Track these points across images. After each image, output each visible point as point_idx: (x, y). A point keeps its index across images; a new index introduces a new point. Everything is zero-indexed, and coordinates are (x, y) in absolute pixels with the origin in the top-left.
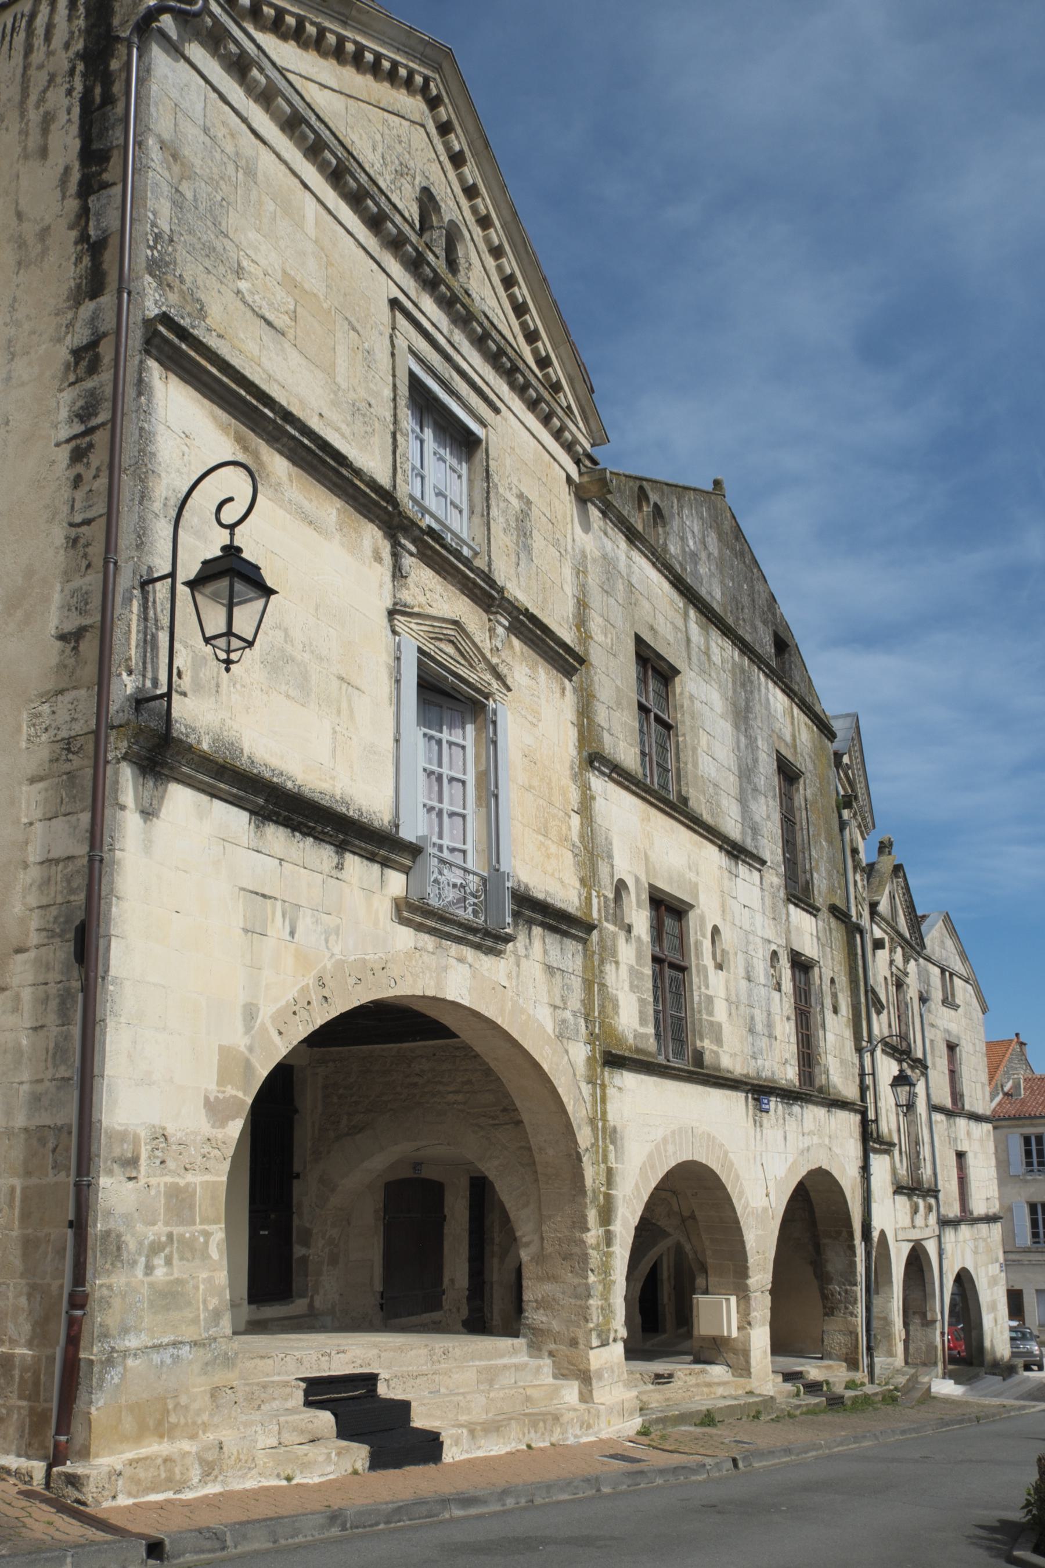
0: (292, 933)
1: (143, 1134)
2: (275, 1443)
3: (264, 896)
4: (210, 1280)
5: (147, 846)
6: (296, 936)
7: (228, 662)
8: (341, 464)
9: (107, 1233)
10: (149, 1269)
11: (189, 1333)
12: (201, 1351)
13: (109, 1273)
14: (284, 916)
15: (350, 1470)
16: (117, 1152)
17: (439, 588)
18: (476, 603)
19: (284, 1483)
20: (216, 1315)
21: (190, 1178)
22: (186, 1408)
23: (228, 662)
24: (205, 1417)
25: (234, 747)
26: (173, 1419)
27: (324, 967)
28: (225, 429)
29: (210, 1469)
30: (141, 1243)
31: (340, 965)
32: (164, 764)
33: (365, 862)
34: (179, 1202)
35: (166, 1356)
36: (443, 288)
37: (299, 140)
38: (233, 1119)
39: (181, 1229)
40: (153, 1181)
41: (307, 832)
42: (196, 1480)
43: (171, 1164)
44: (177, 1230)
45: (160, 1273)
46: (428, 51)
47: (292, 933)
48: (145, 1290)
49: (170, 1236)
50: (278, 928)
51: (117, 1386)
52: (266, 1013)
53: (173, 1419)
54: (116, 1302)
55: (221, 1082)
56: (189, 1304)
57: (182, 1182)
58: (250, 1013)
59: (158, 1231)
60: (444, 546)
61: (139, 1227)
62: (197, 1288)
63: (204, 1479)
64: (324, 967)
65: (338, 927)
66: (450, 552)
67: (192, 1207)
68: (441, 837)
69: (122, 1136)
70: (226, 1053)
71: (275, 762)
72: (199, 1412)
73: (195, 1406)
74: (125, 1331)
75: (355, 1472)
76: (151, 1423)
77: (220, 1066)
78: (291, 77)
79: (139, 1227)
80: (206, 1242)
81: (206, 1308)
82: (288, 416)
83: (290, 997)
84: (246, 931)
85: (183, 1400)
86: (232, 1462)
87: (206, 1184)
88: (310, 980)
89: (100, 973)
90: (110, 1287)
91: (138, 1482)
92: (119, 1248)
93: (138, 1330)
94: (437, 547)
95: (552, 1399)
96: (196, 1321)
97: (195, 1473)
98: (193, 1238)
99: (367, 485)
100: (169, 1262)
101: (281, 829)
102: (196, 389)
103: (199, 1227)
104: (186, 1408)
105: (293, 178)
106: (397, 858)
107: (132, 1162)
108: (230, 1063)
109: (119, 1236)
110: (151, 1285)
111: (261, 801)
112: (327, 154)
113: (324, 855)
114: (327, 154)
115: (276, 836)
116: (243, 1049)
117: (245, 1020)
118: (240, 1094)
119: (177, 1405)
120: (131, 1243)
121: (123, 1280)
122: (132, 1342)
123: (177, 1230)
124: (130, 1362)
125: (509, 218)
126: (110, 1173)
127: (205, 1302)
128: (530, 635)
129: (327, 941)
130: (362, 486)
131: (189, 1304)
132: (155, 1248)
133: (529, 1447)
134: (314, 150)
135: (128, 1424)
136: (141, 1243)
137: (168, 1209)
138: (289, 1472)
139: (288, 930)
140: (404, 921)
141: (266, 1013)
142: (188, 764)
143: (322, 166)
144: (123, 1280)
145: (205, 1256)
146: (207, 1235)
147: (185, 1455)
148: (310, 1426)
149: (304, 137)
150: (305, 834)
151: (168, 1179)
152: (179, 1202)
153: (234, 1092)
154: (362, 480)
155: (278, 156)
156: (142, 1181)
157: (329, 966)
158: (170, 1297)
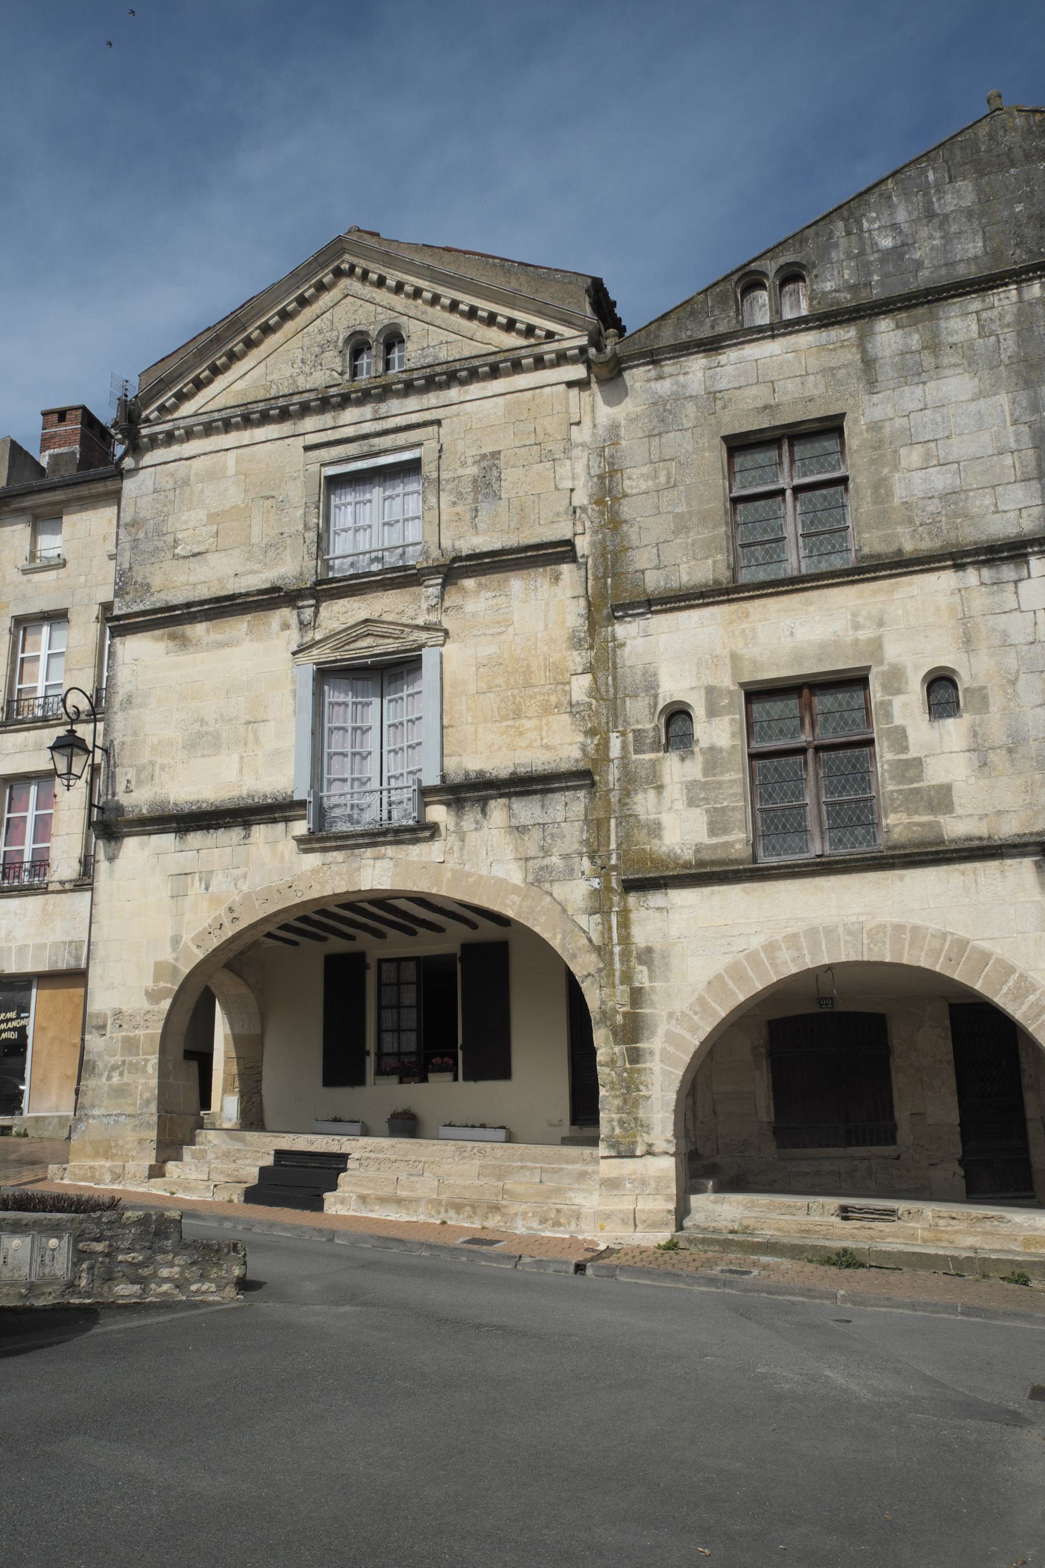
0: (207, 889)
1: (109, 1013)
2: (206, 1178)
3: (186, 874)
4: (146, 1084)
5: (111, 874)
6: (210, 889)
7: (68, 786)
8: (235, 599)
9: (89, 1061)
10: (109, 1078)
11: (129, 1110)
12: (133, 1120)
13: (87, 1079)
14: (200, 880)
15: (227, 1199)
16: (94, 1023)
17: (356, 605)
18: (405, 587)
19: (168, 1195)
20: (148, 1102)
21: (137, 1032)
22: (122, 1147)
23: (68, 786)
24: (134, 1153)
25: (164, 803)
26: (114, 1151)
27: (234, 901)
28: (160, 639)
29: (117, 1178)
30: (106, 1066)
31: (247, 896)
32: (115, 833)
33: (270, 825)
34: (130, 1045)
35: (111, 1120)
36: (353, 396)
37: (217, 431)
38: (165, 998)
39: (131, 1058)
40: (114, 1035)
41: (217, 827)
42: (108, 1181)
43: (125, 1026)
44: (127, 1059)
45: (116, 1079)
46: (320, 260)
47: (207, 889)
48: (106, 1088)
49: (124, 1062)
50: (196, 887)
51: (84, 1131)
52: (187, 937)
53: (114, 1151)
54: (90, 1093)
55: (156, 980)
56: (131, 1095)
57: (132, 1035)
58: (176, 941)
59: (118, 1059)
60: (340, 580)
61: (106, 1058)
62: (137, 1087)
63: (113, 1181)
64: (234, 901)
65: (246, 874)
66: (350, 580)
67: (137, 1047)
68: (345, 780)
69: (98, 1015)
70: (159, 966)
71: (193, 798)
72: (130, 1150)
73: (128, 1146)
74: (93, 1106)
75: (231, 1201)
76: (101, 1151)
77: (155, 972)
78: (200, 411)
79: (106, 1058)
80: (146, 1065)
81: (141, 1097)
82: (188, 605)
83: (206, 925)
84: (172, 897)
85: (121, 1142)
86: (130, 1176)
87: (146, 1036)
88: (222, 911)
89: (976, 843)
90: (87, 1086)
91: (75, 1175)
92: (94, 1068)
93: (100, 1106)
94: (334, 585)
95: (548, 1197)
96: (134, 1104)
97: (108, 1177)
98: (138, 1062)
99: (258, 595)
100: (121, 1074)
101: (199, 832)
102: (142, 632)
103: (141, 1057)
104: (122, 1147)
105: (219, 454)
106: (292, 813)
107: (104, 1027)
108: (161, 970)
109: (94, 1062)
110: (110, 1086)
111: (174, 825)
112: (233, 420)
113: (236, 834)
114: (233, 420)
115: (195, 839)
116: (171, 960)
117: (172, 944)
118: (169, 985)
119: (116, 1145)
120: (100, 1065)
121: (94, 1083)
122: (96, 1112)
123: (127, 1059)
124: (90, 1121)
125: (429, 273)
126: (90, 1033)
127: (141, 1095)
128: (484, 567)
129: (236, 884)
130: (255, 598)
131: (131, 1095)
132: (114, 1068)
133: (444, 1223)
134: (228, 426)
135: (89, 1149)
136: (106, 1066)
137: (123, 1048)
138: (174, 1190)
139: (203, 886)
140: (306, 851)
141: (187, 937)
142: (125, 826)
143: (238, 427)
144: (94, 1083)
145: (144, 1070)
146: (147, 1061)
147: (102, 1167)
148: (235, 1173)
149: (217, 428)
150: (216, 829)
151: (124, 1034)
152: (130, 1045)
153: (165, 985)
154: (253, 596)
155: (205, 454)
156: (108, 1036)
157: (237, 898)
158: (120, 1092)
